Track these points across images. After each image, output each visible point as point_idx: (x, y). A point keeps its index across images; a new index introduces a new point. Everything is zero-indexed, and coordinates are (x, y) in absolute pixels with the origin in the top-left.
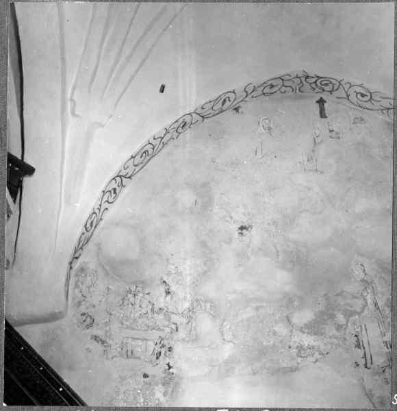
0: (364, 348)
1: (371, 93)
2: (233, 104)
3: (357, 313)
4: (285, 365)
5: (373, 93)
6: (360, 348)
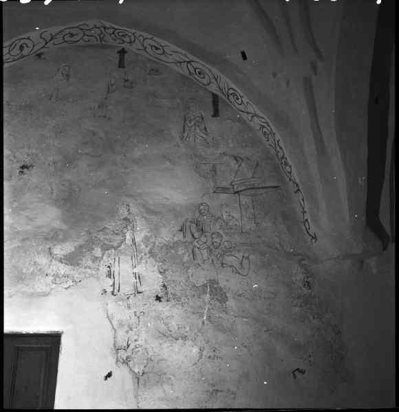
0: (114, 278)
2: (34, 51)
3: (114, 247)
4: (39, 290)
6: (110, 278)
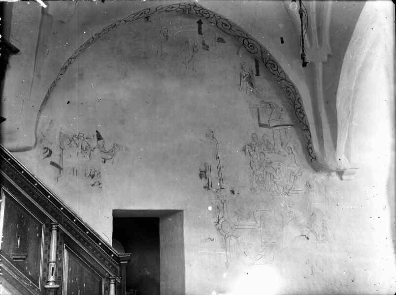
1: (231, 26)
5: (107, 159)
